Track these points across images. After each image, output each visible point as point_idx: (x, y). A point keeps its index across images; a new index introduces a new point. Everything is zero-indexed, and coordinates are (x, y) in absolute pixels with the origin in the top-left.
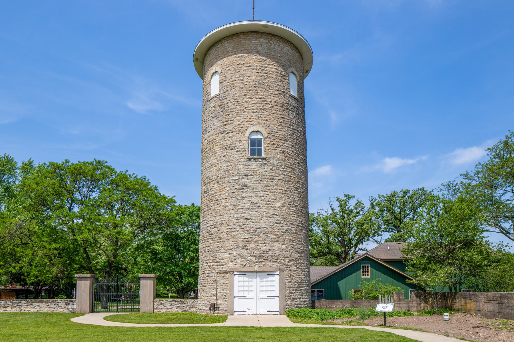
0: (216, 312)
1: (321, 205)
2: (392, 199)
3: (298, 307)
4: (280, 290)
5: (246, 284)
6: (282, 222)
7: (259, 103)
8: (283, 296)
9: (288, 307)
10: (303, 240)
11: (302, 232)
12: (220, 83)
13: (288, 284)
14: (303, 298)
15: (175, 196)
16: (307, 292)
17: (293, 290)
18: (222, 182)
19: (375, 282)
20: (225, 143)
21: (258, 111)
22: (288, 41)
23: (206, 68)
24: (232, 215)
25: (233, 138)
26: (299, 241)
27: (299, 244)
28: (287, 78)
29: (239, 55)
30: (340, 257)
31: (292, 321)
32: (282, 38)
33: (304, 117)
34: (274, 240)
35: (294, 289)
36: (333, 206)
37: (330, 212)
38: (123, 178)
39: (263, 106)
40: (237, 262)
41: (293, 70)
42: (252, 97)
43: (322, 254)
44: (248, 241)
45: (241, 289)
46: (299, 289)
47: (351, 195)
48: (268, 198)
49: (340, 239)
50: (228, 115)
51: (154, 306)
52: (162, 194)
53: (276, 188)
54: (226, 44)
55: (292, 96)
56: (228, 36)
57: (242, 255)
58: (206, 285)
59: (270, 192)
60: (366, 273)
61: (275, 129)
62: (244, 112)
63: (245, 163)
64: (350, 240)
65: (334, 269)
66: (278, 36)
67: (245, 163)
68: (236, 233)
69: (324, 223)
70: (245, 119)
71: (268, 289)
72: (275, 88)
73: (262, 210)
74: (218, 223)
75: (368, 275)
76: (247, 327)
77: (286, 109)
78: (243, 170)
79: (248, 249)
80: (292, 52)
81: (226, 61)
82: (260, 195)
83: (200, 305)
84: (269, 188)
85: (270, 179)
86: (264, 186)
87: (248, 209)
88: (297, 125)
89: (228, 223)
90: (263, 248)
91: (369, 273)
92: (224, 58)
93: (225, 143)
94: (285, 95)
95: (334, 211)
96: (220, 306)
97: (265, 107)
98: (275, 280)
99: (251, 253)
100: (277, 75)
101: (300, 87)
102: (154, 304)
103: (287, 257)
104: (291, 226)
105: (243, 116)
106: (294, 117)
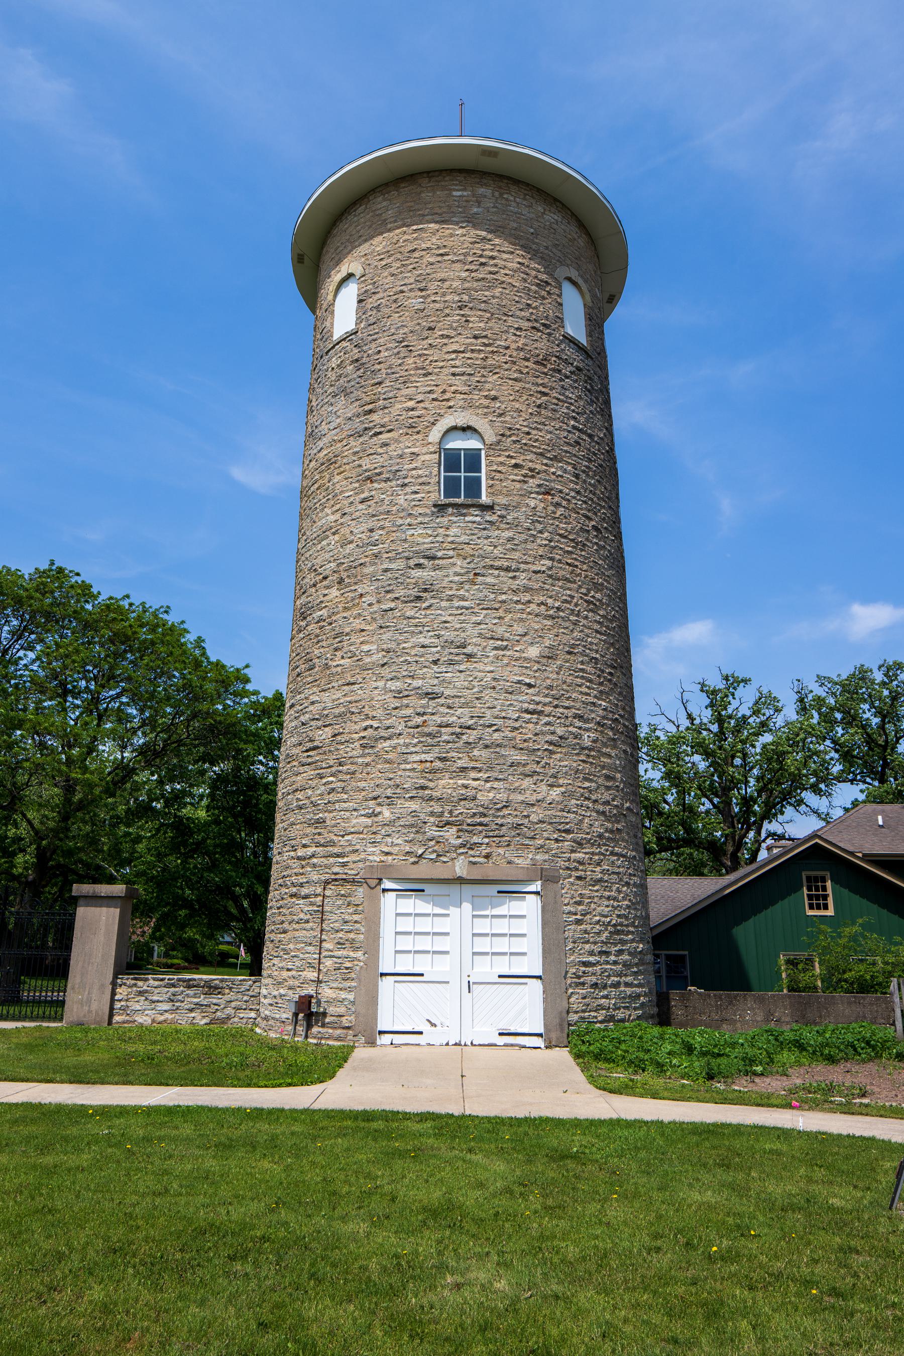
0: (315, 1030)
1: (667, 688)
2: (854, 687)
3: (610, 1019)
4: (547, 952)
5: (424, 925)
6: (548, 709)
7: (473, 351)
8: (555, 977)
9: (574, 1017)
10: (618, 776)
11: (615, 747)
12: (360, 301)
13: (573, 931)
14: (627, 985)
15: (247, 666)
16: (642, 962)
17: (591, 953)
18: (352, 580)
19: (856, 929)
20: (366, 463)
21: (469, 370)
22: (556, 200)
23: (323, 273)
24: (380, 684)
25: (393, 447)
26: (608, 778)
27: (608, 788)
28: (557, 291)
29: (415, 227)
30: (721, 856)
31: (592, 1080)
32: (539, 190)
33: (607, 402)
34: (521, 769)
35: (597, 948)
36: (690, 708)
37: (685, 723)
38: (113, 610)
39: (485, 359)
40: (393, 845)
41: (574, 274)
42: (452, 333)
43: (666, 844)
44: (433, 771)
45: (405, 943)
46: (613, 949)
47: (741, 675)
48: (500, 630)
49: (716, 800)
50: (380, 383)
51: (112, 1001)
52: (213, 659)
53: (527, 597)
54: (380, 203)
55: (571, 341)
56: (387, 184)
57: (410, 820)
58: (286, 925)
59: (508, 611)
60: (819, 901)
61: (520, 422)
62: (425, 375)
63: (426, 520)
64: (747, 802)
65: (718, 887)
66: (528, 185)
67: (426, 520)
68: (395, 741)
69: (669, 756)
70: (430, 392)
71: (502, 945)
72: (518, 313)
73: (480, 666)
74: (337, 711)
75: (826, 907)
76: (407, 1116)
77: (554, 370)
78: (421, 540)
79: (431, 799)
80: (568, 230)
81: (379, 243)
82: (474, 619)
83: (264, 1005)
84: (504, 597)
85: (508, 569)
86: (486, 592)
87: (435, 662)
88: (587, 420)
89: (366, 710)
90: (483, 798)
91: (830, 901)
92: (372, 237)
93: (366, 463)
94: (549, 334)
95: (697, 722)
96: (331, 1010)
97: (490, 362)
98: (529, 908)
99: (441, 814)
100: (525, 280)
101: (596, 321)
102: (113, 994)
103: (568, 831)
104: (578, 723)
105: (423, 384)
106: (580, 397)
